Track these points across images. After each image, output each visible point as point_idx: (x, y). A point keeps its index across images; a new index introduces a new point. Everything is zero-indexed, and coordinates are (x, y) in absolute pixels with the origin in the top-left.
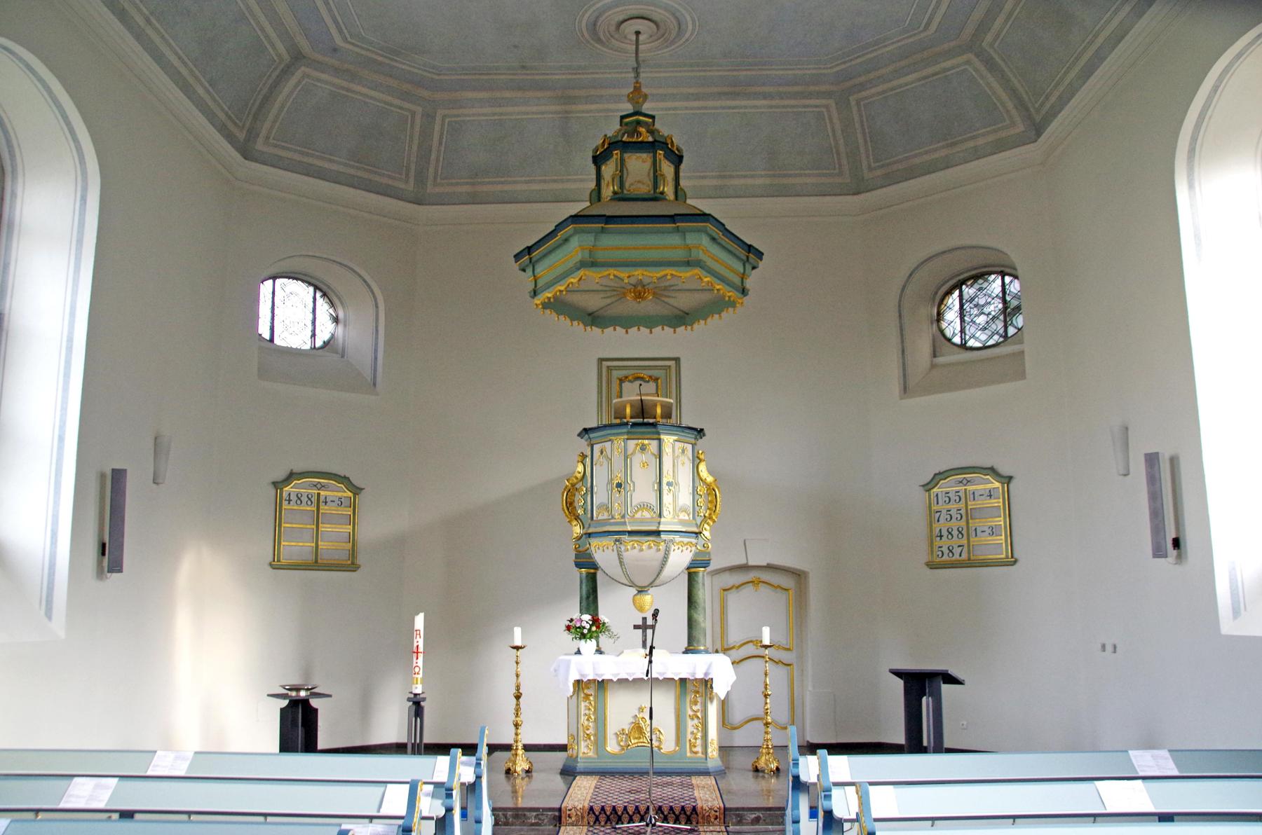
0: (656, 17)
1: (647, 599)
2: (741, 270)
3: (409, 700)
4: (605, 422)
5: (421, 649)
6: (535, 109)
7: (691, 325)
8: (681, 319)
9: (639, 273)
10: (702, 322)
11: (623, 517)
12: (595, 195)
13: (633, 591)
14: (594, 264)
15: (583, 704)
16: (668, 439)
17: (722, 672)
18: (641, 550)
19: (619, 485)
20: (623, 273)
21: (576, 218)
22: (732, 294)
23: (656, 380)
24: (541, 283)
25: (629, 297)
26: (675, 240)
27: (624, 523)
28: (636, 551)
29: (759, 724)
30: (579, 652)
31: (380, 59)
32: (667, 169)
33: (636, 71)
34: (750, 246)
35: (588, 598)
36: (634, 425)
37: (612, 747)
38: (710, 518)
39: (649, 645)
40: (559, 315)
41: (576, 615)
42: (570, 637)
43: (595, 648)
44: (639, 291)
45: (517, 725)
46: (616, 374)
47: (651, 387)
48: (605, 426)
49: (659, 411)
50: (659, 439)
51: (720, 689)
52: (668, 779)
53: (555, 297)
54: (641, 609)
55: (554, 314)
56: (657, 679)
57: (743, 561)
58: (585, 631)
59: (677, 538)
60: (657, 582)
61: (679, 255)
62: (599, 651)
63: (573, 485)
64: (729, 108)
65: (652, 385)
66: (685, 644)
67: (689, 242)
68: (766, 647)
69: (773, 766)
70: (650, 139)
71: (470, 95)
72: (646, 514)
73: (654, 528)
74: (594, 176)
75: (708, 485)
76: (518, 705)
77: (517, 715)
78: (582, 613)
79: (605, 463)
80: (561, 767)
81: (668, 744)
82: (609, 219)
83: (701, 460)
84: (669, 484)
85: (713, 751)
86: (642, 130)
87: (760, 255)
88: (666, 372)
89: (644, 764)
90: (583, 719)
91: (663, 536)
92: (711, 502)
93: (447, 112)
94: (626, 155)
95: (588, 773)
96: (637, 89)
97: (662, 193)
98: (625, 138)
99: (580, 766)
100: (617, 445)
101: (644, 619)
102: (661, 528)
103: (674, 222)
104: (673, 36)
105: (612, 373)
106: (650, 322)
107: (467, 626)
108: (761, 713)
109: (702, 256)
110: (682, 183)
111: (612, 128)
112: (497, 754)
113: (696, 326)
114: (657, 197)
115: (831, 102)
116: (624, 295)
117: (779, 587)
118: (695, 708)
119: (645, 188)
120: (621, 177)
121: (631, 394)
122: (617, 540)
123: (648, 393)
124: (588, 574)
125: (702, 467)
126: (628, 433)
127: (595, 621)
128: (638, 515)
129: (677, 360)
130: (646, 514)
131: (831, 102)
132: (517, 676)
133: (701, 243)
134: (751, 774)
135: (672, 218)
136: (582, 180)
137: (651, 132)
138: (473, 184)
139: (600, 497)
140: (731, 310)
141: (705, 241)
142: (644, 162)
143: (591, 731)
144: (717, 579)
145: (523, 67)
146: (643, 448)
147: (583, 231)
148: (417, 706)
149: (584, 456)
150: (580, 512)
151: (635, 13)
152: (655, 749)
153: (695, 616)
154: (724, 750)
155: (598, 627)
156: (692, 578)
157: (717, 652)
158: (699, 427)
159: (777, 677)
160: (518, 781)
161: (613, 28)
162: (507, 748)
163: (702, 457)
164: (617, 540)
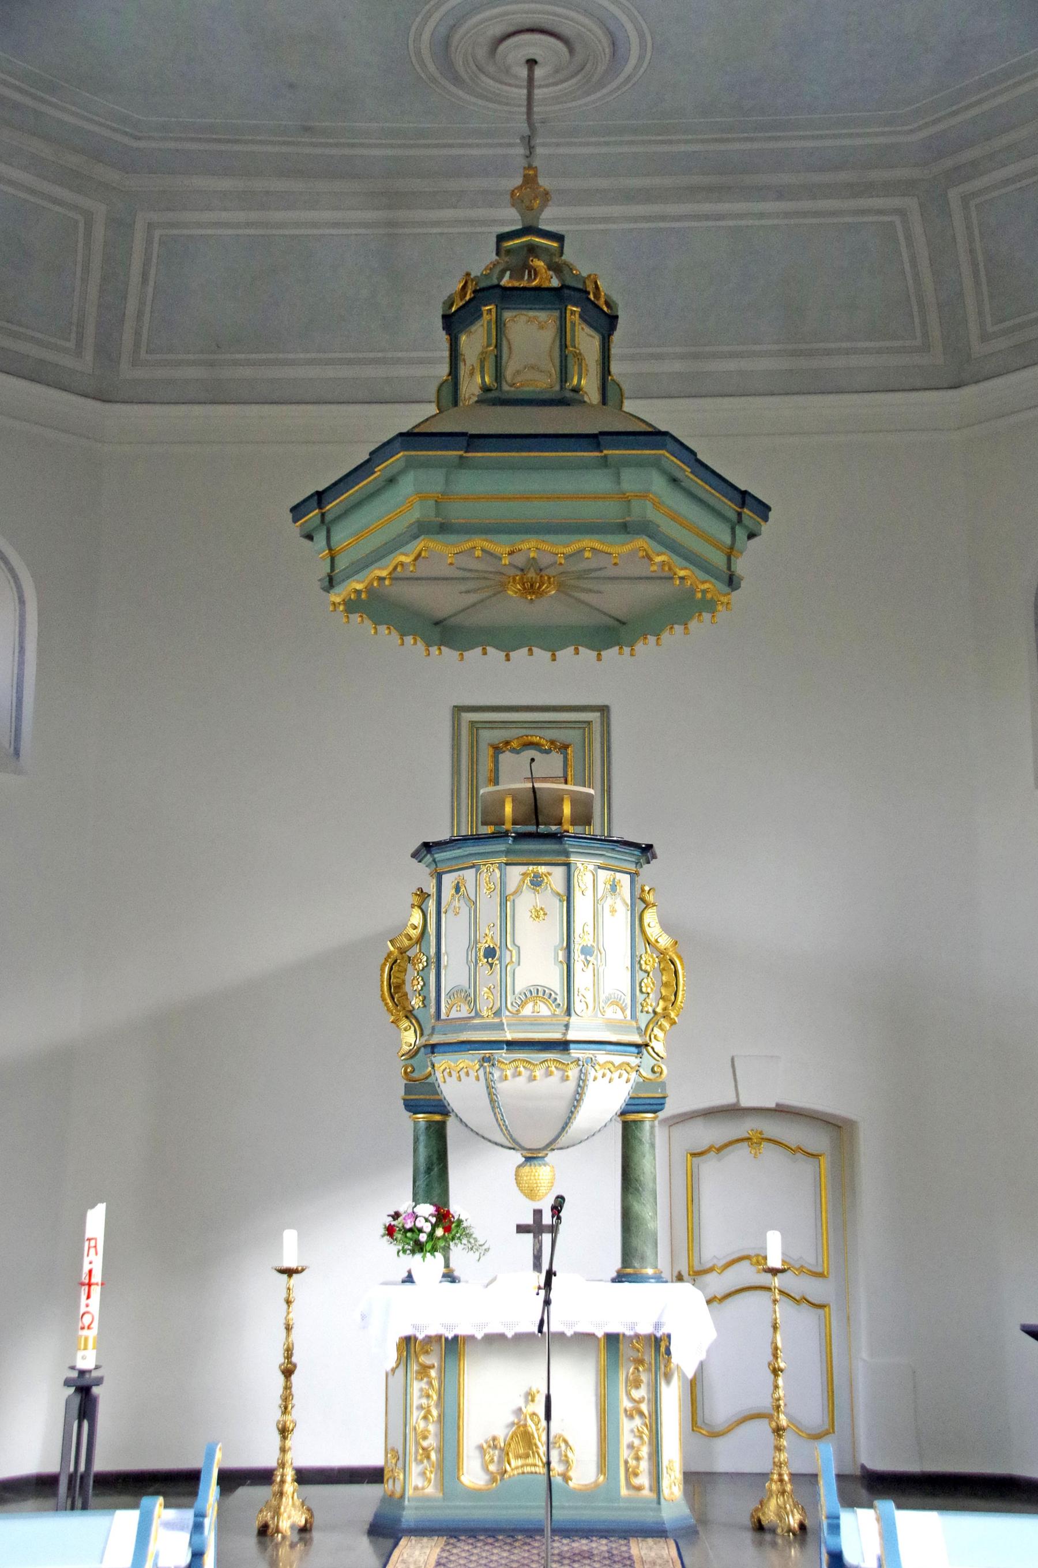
0: (565, 30)
1: (542, 1173)
2: (728, 540)
3: (67, 1383)
4: (465, 831)
5: (97, 1278)
6: (327, 215)
7: (631, 645)
8: (611, 633)
9: (530, 546)
10: (652, 639)
11: (498, 1013)
12: (447, 391)
13: (518, 1158)
14: (444, 528)
15: (417, 1386)
16: (587, 870)
17: (679, 1313)
18: (532, 1079)
19: (490, 953)
20: (500, 546)
21: (411, 438)
22: (709, 586)
23: (564, 748)
24: (341, 564)
25: (512, 592)
26: (598, 482)
27: (500, 1027)
28: (522, 1080)
29: (763, 1427)
30: (409, 1279)
31: (17, 97)
32: (587, 341)
33: (529, 142)
34: (745, 493)
35: (429, 1170)
36: (521, 837)
37: (473, 1475)
39: (545, 1266)
40: (377, 622)
41: (405, 1205)
42: (394, 1248)
43: (442, 1270)
44: (532, 581)
45: (284, 1432)
46: (488, 736)
47: (550, 764)
48: (465, 839)
49: (567, 810)
50: (568, 865)
51: (686, 1358)
52: (582, 1545)
53: (369, 589)
54: (530, 1193)
55: (368, 623)
56: (562, 1335)
57: (729, 1099)
58: (423, 1237)
59: (602, 1056)
60: (563, 1140)
61: (611, 511)
62: (450, 1277)
63: (402, 951)
64: (707, 217)
65: (556, 758)
66: (618, 1265)
67: (626, 486)
68: (774, 1272)
69: (794, 1521)
70: (555, 283)
71: (200, 182)
72: (544, 1010)
74: (447, 354)
75: (662, 953)
76: (287, 1388)
77: (285, 1410)
78: (416, 1201)
79: (465, 910)
80: (367, 1527)
81: (583, 1472)
82: (472, 441)
83: (647, 905)
84: (586, 951)
85: (673, 1487)
86: (539, 264)
87: (763, 510)
88: (580, 734)
89: (534, 1511)
90: (416, 1415)
91: (575, 1053)
92: (665, 985)
93: (154, 217)
94: (507, 315)
95: (423, 1531)
96: (530, 180)
97: (576, 390)
98: (505, 281)
99: (409, 1516)
100: (485, 879)
101: (538, 1213)
102: (571, 1036)
103: (598, 448)
104: (601, 68)
105: (482, 736)
106: (552, 638)
107: (192, 1226)
108: (765, 1403)
109: (652, 515)
110: (616, 368)
111: (482, 261)
112: (245, 1493)
113: (639, 646)
114: (566, 398)
115: (911, 203)
116: (503, 587)
117: (800, 1149)
118: (636, 1394)
119: (545, 382)
120: (498, 358)
121: (515, 777)
122: (484, 1059)
123: (547, 773)
124: (430, 1124)
125: (651, 917)
126: (508, 853)
127: (443, 1217)
128: (527, 1010)
129: (604, 710)
130: (544, 1010)
131: (911, 203)
132: (288, 1328)
133: (649, 487)
134: (748, 1536)
135: (594, 440)
136: (421, 361)
137: (556, 268)
138: (212, 364)
140: (706, 616)
141: (658, 484)
142: (541, 327)
143: (431, 1442)
144: (678, 1131)
145: (307, 129)
146: (537, 882)
147: (426, 464)
148: (84, 1396)
149: (423, 895)
150: (416, 1002)
151: (529, 21)
152: (557, 1480)
153: (636, 1207)
154: (696, 1481)
155: (447, 1229)
156: (629, 1132)
157: (680, 1278)
158: (644, 841)
159: (799, 1331)
160: (283, 1551)
161: (482, 53)
162: (263, 1477)
163: (650, 898)
164: (484, 1059)
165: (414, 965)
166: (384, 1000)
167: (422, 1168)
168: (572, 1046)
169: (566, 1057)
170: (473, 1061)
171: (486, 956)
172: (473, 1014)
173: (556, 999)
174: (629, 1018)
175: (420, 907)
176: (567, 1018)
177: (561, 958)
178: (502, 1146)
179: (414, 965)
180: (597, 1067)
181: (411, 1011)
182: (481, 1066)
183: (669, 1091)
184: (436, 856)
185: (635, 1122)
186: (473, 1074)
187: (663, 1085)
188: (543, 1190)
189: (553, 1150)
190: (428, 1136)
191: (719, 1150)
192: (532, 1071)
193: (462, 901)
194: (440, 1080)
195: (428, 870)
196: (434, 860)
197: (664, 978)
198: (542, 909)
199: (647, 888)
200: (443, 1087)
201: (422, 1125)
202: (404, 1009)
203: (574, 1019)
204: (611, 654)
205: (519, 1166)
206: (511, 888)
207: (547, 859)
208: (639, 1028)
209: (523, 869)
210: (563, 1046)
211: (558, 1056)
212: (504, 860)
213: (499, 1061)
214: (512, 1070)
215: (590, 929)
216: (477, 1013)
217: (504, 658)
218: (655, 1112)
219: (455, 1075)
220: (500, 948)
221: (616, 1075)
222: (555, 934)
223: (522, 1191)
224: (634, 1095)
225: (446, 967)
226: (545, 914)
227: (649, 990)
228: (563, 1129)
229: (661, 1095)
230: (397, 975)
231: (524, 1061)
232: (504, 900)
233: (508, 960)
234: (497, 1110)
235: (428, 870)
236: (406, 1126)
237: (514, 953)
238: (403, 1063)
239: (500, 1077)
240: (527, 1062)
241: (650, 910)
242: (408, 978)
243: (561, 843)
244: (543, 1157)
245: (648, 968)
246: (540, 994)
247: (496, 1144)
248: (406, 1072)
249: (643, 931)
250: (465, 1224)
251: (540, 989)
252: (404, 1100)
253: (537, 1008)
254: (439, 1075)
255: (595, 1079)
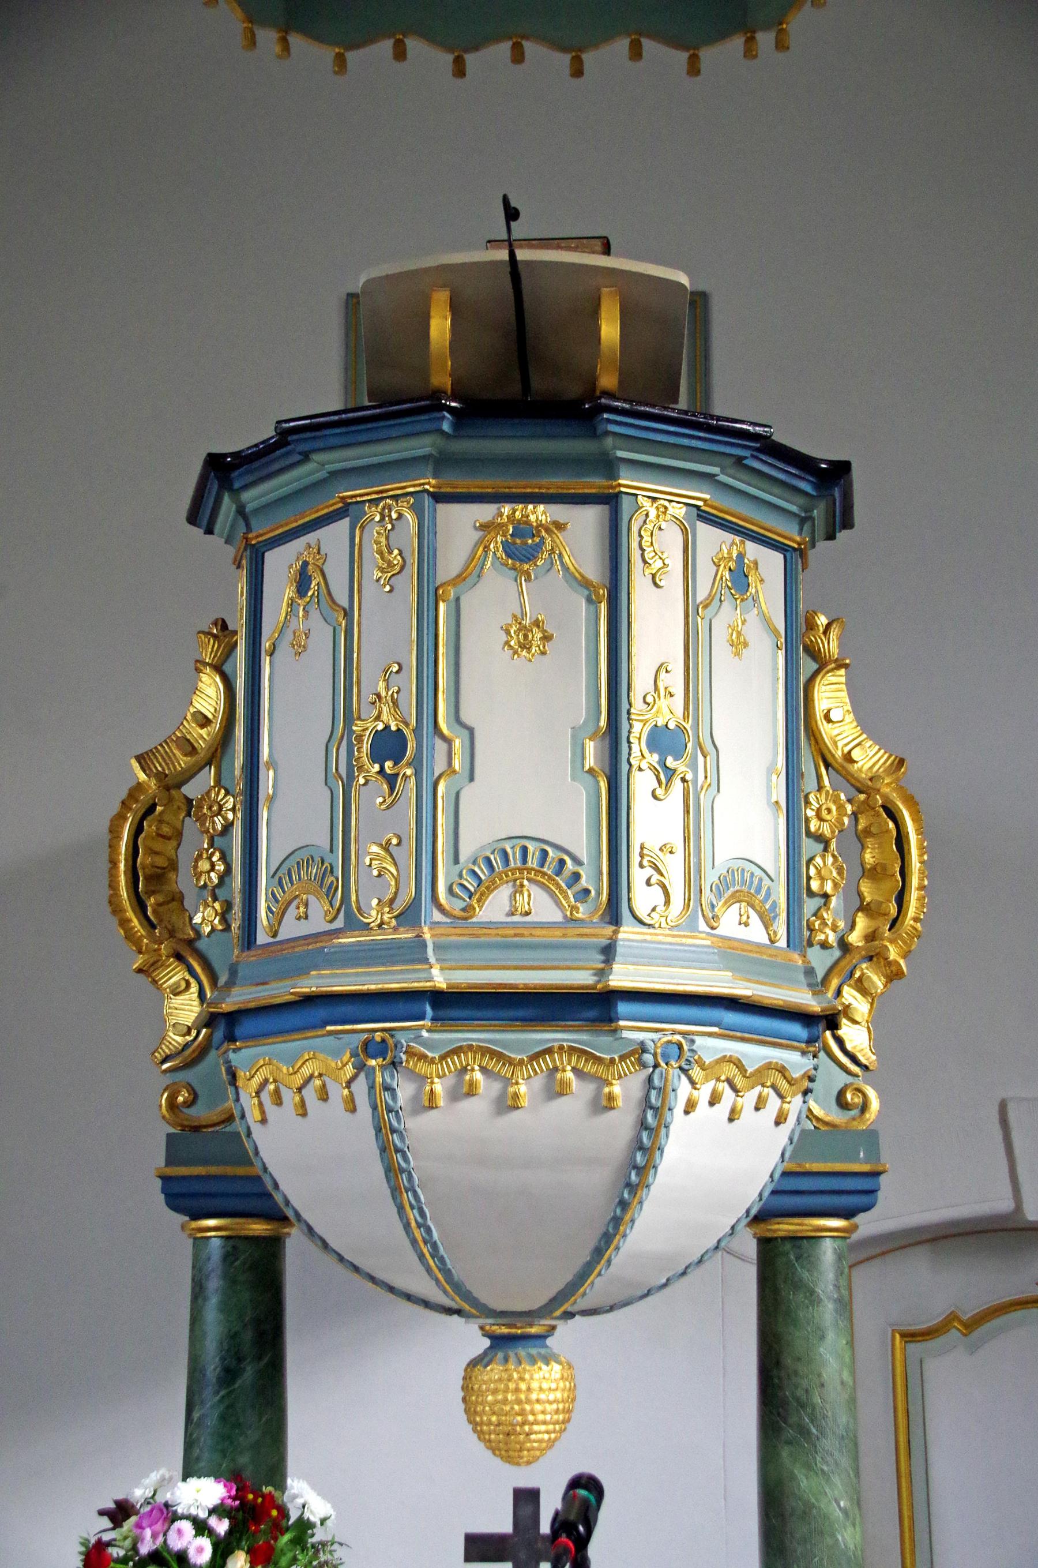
1: (543, 1382)
7: (777, 23)
11: (409, 916)
13: (469, 1338)
16: (663, 516)
18: (507, 1104)
19: (389, 746)
35: (229, 1375)
38: (874, 956)
50: (611, 500)
54: (506, 1442)
63: (171, 784)
72: (542, 906)
73: (581, 978)
75: (862, 788)
79: (321, 635)
83: (822, 663)
84: (662, 740)
91: (634, 1029)
92: (874, 873)
102: (622, 977)
122: (369, 1048)
124: (234, 1243)
125: (831, 695)
126: (440, 463)
130: (542, 906)
139: (293, 815)
150: (205, 917)
153: (805, 1483)
158: (823, 450)
163: (832, 646)
164: (369, 1048)
165: (201, 819)
166: (117, 909)
167: (212, 1368)
168: (623, 1008)
169: (606, 1040)
170: (337, 1054)
171: (377, 756)
172: (339, 923)
173: (577, 876)
174: (782, 943)
175: (218, 669)
176: (610, 930)
177: (590, 762)
178: (426, 1304)
179: (201, 819)
180: (696, 1072)
181: (190, 943)
182: (360, 1067)
183: (887, 1159)
184: (246, 496)
185: (795, 1239)
186: (338, 1093)
187: (871, 1137)
188: (541, 1433)
189: (569, 1315)
190: (231, 1281)
191: (972, 1325)
192: (508, 1082)
193: (315, 614)
194: (253, 1115)
195: (230, 551)
196: (241, 511)
197: (868, 857)
198: (537, 623)
199: (822, 620)
200: (257, 1130)
201: (216, 1246)
202: (172, 934)
203: (628, 932)
204: (723, 55)
205: (473, 1363)
206: (451, 561)
207: (553, 482)
208: (810, 972)
209: (485, 512)
210: (599, 1006)
211: (584, 1037)
212: (430, 483)
213: (410, 1053)
214: (451, 1080)
215: (675, 680)
216: (350, 918)
217: (450, 67)
218: (848, 1214)
219: (289, 1098)
220: (417, 731)
221: (750, 1098)
222: (577, 700)
223: (480, 1435)
224: (793, 1167)
225: (271, 799)
226: (547, 638)
227: (829, 888)
228: (598, 1253)
229: (866, 1168)
230: (158, 846)
231: (485, 1051)
232: (429, 595)
233: (440, 767)
234: (407, 1198)
235: (230, 551)
236: (169, 1255)
237: (457, 744)
238: (167, 1080)
239: (416, 1098)
240: (493, 1054)
241: (830, 678)
242: (185, 855)
243: (594, 434)
244: (541, 1337)
245: (826, 830)
246: (533, 862)
247: (409, 1297)
248: (172, 1105)
249: (813, 735)
250: (319, 1535)
251: (531, 847)
252: (165, 1179)
253: (522, 903)
254: (249, 1103)
255: (690, 1107)
